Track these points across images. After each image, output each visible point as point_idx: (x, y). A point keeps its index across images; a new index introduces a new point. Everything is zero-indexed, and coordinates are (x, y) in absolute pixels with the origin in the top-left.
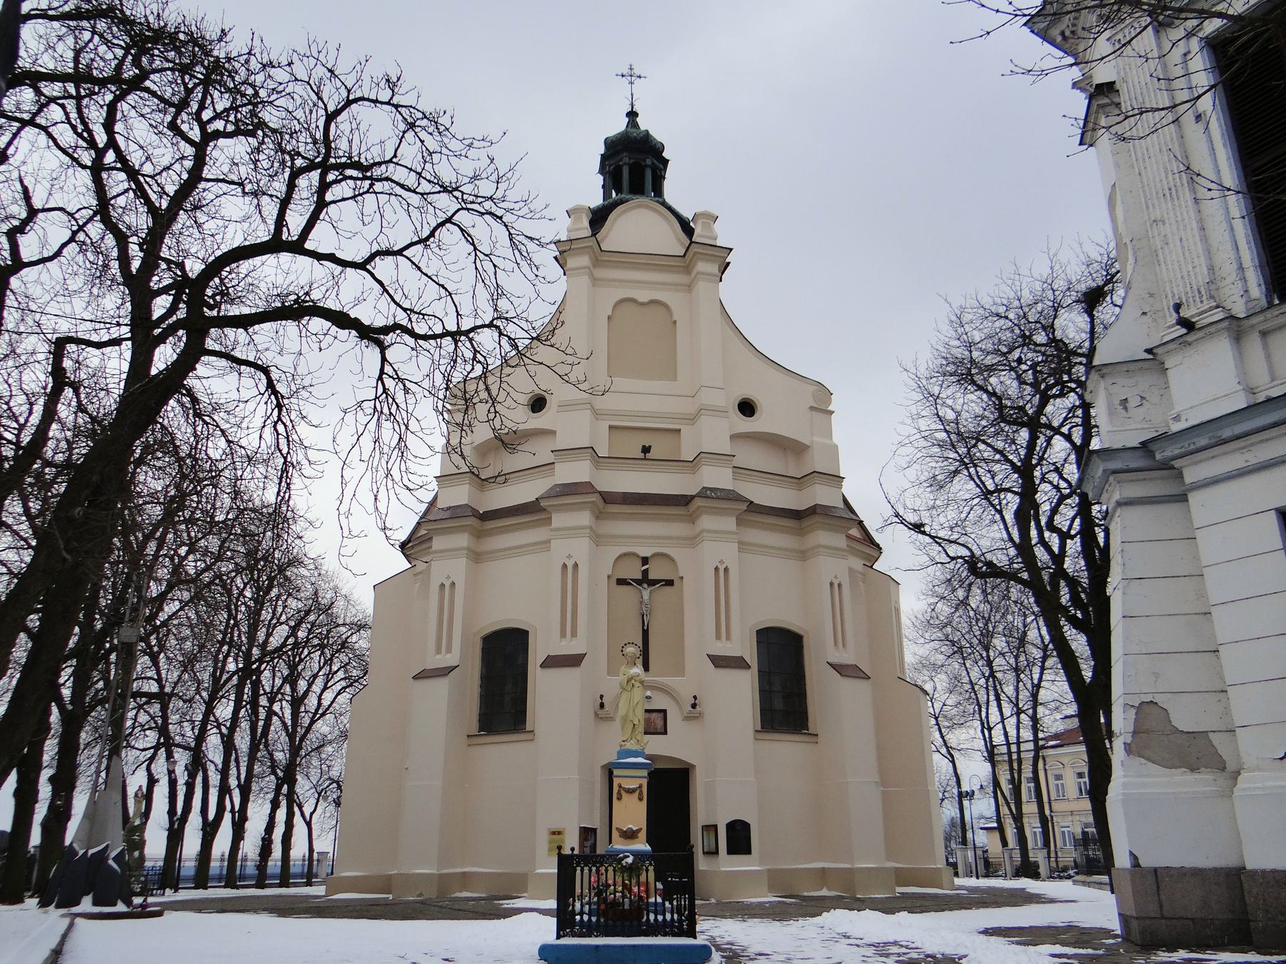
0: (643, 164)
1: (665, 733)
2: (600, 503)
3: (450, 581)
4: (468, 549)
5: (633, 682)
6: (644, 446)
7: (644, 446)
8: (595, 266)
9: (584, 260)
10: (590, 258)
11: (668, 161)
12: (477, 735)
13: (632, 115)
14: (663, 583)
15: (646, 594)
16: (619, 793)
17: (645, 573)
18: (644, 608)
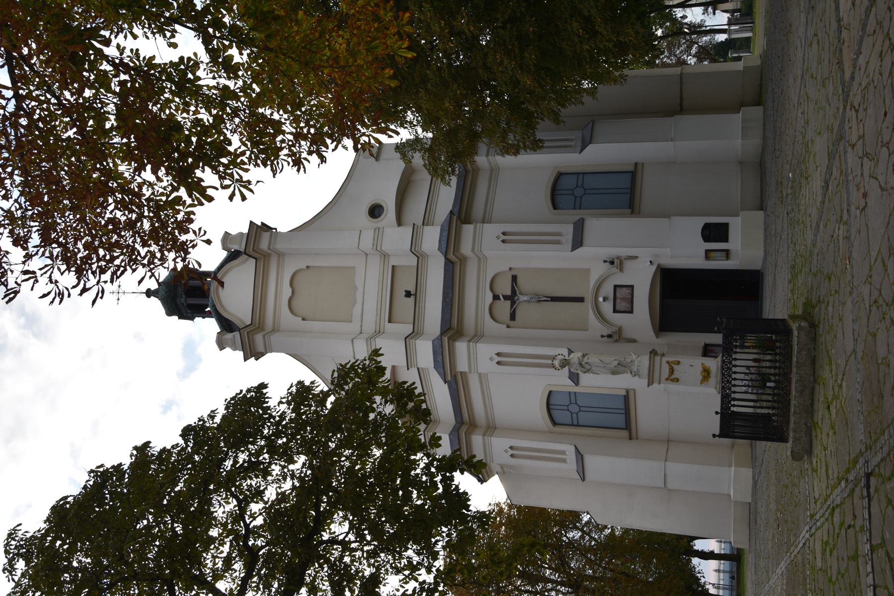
2: (451, 333)
3: (509, 450)
5: (584, 363)
16: (673, 380)
17: (506, 298)
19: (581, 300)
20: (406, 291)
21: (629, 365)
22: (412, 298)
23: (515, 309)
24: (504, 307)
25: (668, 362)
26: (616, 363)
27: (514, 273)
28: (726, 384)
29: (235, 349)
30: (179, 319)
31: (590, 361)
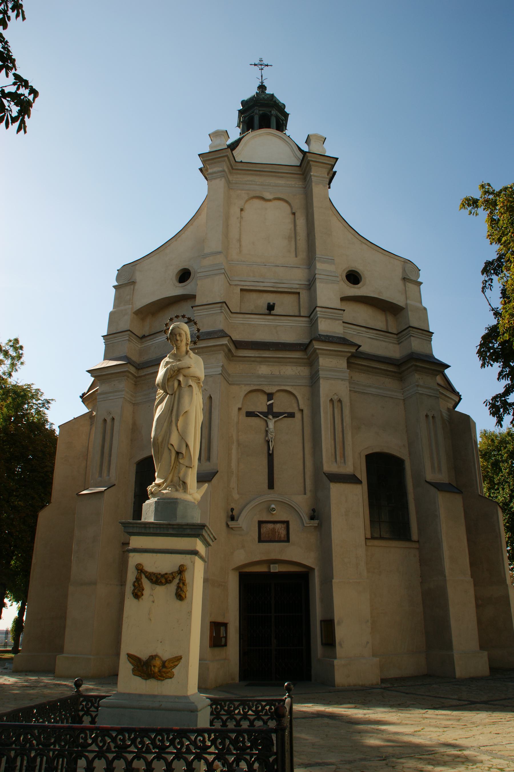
1: (288, 540)
2: (232, 347)
3: (111, 417)
6: (269, 304)
7: (269, 304)
11: (288, 114)
12: (208, 563)
15: (271, 425)
17: (270, 407)
19: (271, 485)
25: (181, 570)
29: (210, 146)
30: (239, 111)
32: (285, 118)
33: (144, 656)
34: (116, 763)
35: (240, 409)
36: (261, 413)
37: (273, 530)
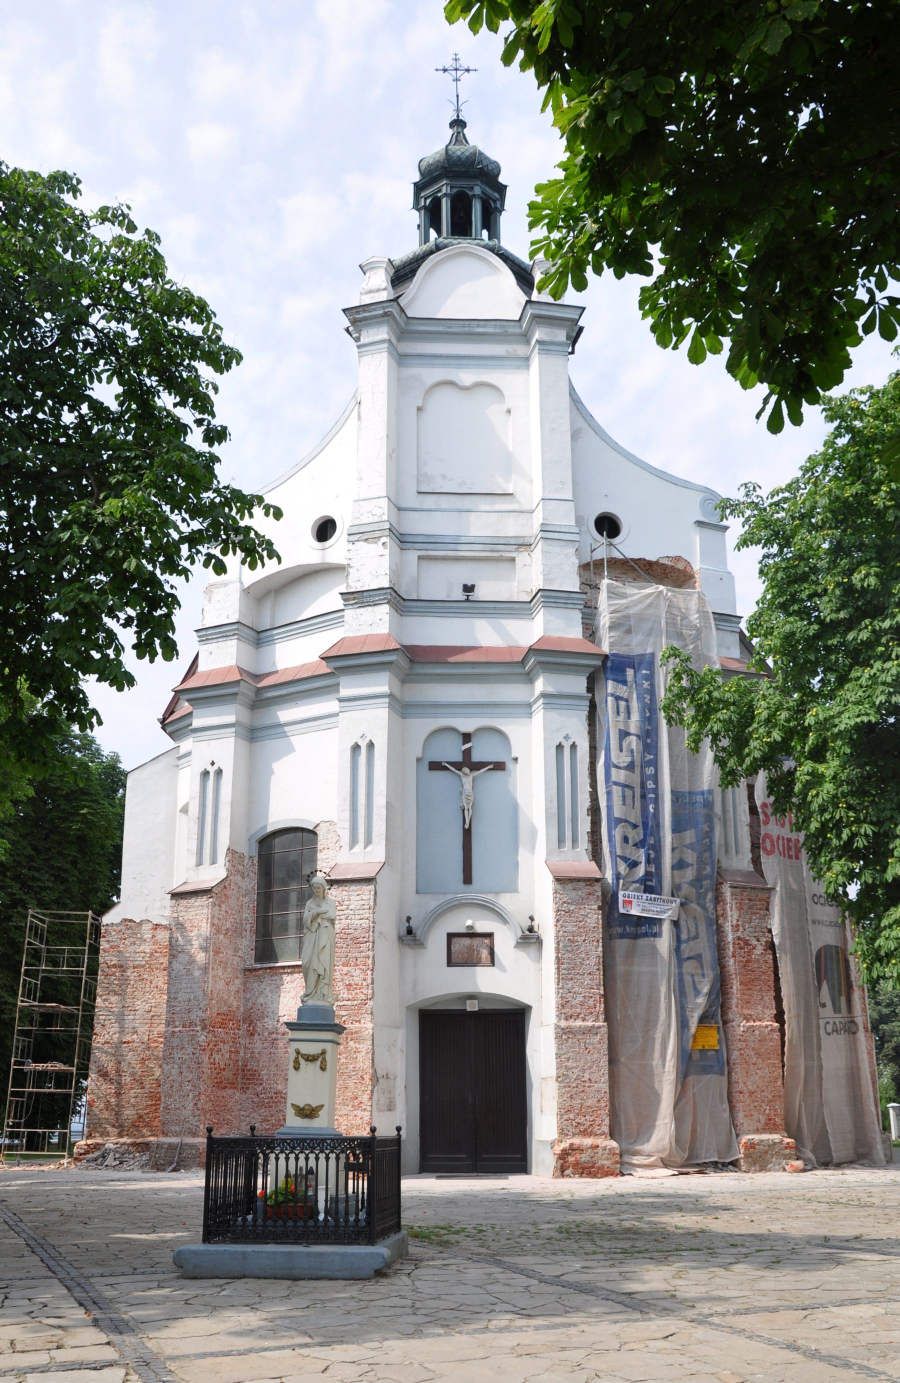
0: (470, 193)
4: (391, 696)
5: (319, 920)
8: (399, 339)
9: (382, 333)
10: (391, 328)
11: (506, 187)
13: (458, 124)
14: (491, 766)
16: (296, 1061)
17: (467, 753)
18: (464, 801)
19: (468, 879)
20: (473, 586)
21: (319, 992)
22: (459, 595)
23: (447, 769)
24: (452, 751)
25: (324, 1053)
26: (321, 972)
27: (509, 765)
28: (289, 1144)
30: (415, 184)
31: (322, 929)
32: (499, 194)
33: (302, 1106)
34: (290, 1155)
35: (418, 760)
36: (452, 764)
37: (470, 948)
